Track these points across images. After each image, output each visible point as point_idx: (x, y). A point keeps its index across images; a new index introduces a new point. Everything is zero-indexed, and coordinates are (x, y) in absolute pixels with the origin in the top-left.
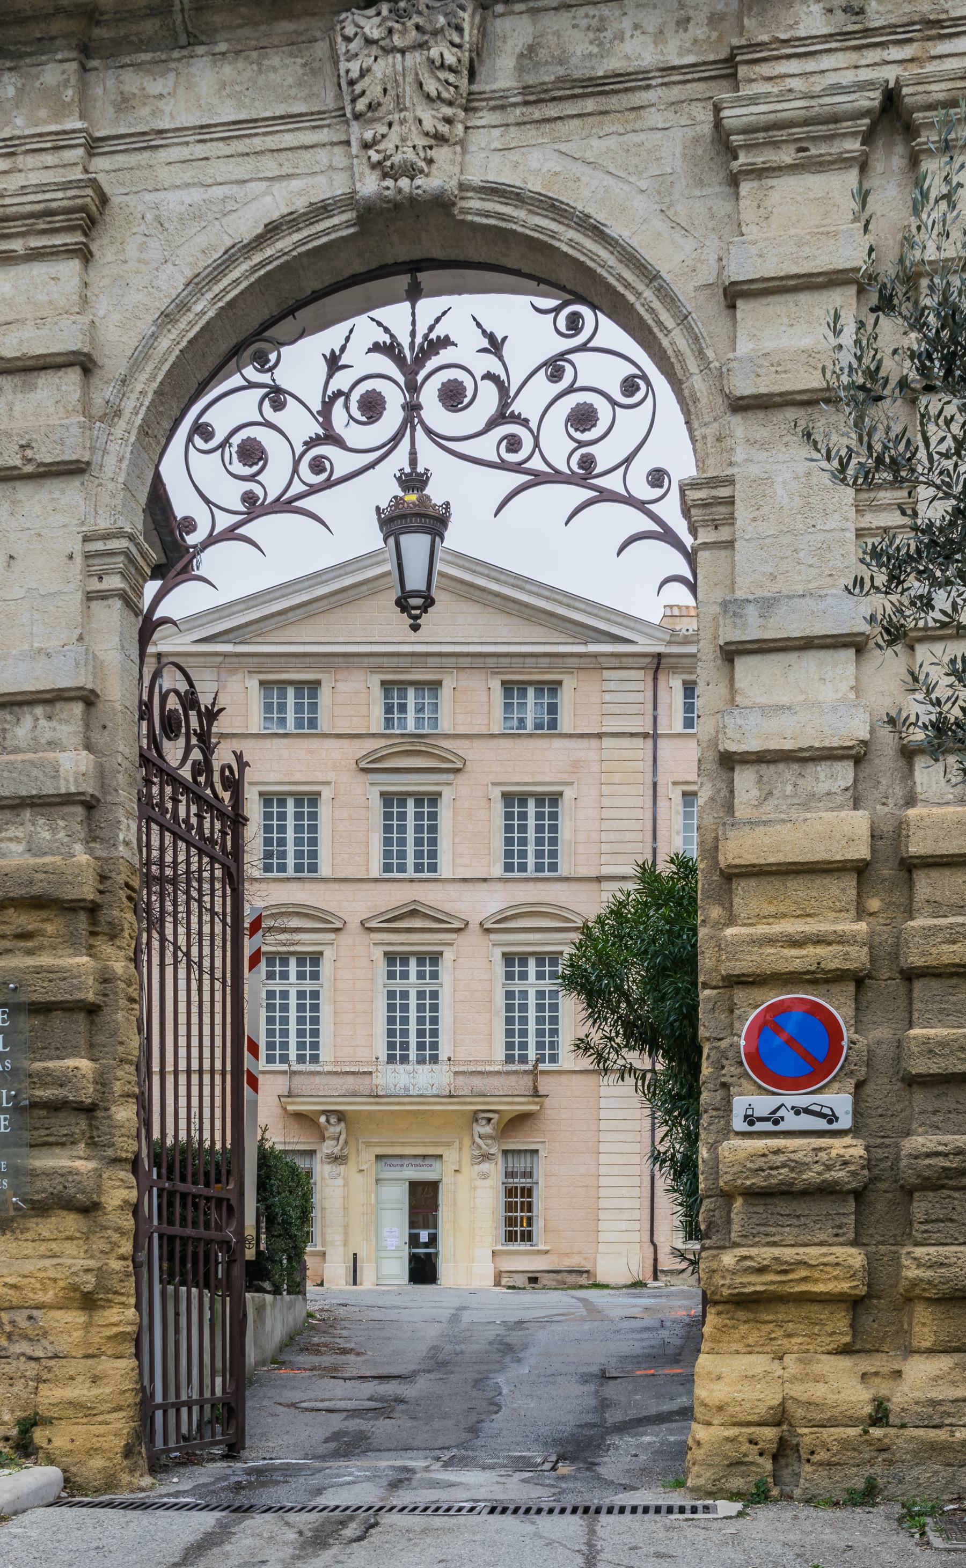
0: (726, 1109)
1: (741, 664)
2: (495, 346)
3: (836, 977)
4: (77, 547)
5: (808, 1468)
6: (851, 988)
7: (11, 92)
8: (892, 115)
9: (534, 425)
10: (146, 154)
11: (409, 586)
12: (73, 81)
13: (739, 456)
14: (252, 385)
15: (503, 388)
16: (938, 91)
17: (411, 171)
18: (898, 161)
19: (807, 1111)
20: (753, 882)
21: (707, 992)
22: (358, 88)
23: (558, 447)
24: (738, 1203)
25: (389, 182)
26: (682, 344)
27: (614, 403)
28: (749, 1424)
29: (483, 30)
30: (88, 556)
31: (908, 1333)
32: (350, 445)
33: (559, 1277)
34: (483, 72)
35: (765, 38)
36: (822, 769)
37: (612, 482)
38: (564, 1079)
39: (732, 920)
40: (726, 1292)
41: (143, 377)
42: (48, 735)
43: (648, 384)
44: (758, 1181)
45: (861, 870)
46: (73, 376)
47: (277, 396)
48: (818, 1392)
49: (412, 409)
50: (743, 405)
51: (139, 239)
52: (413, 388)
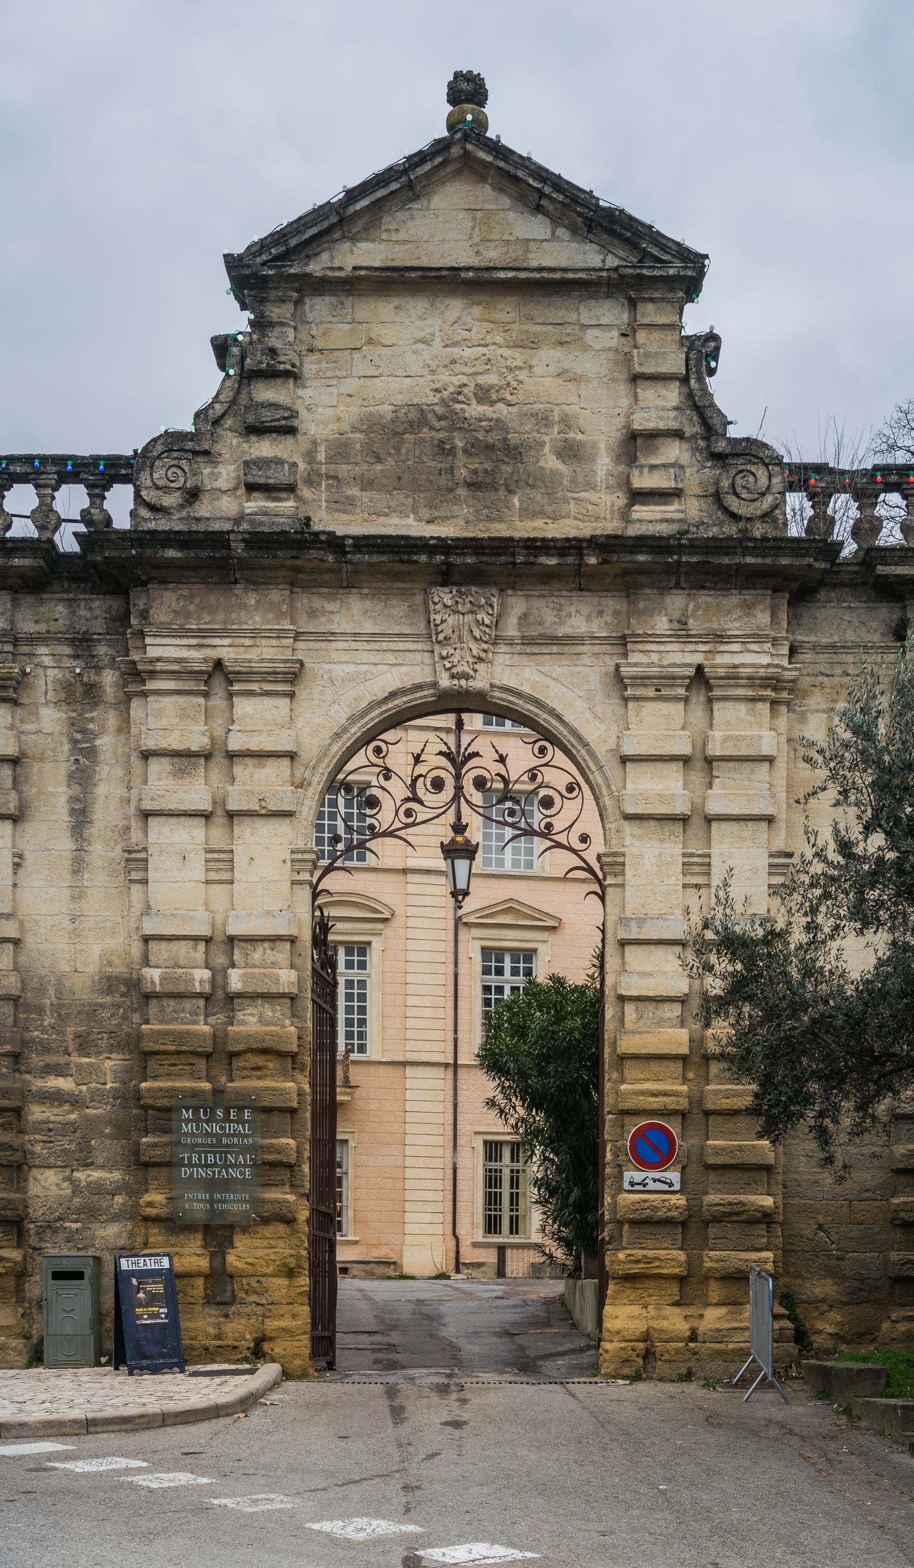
0: (620, 1177)
1: (628, 950)
2: (502, 759)
3: (674, 1113)
4: (288, 857)
5: (660, 1363)
6: (680, 1118)
7: (253, 602)
8: (700, 678)
10: (325, 643)
11: (458, 887)
12: (287, 601)
13: (628, 842)
16: (721, 672)
17: (467, 677)
18: (702, 699)
19: (659, 1180)
20: (633, 1062)
21: (610, 1116)
22: (440, 629)
24: (626, 1227)
25: (456, 682)
26: (600, 779)
27: (562, 796)
28: (631, 1341)
29: (502, 605)
30: (293, 861)
31: (706, 1295)
33: (368, 1268)
34: (501, 625)
35: (640, 632)
36: (667, 1006)
38: (372, 1069)
39: (623, 1081)
40: (620, 1273)
41: (323, 765)
42: (272, 959)
43: (580, 788)
44: (635, 1216)
45: (684, 1058)
46: (286, 762)
48: (664, 1324)
49: (459, 789)
50: (628, 817)
51: (321, 688)
52: (458, 777)
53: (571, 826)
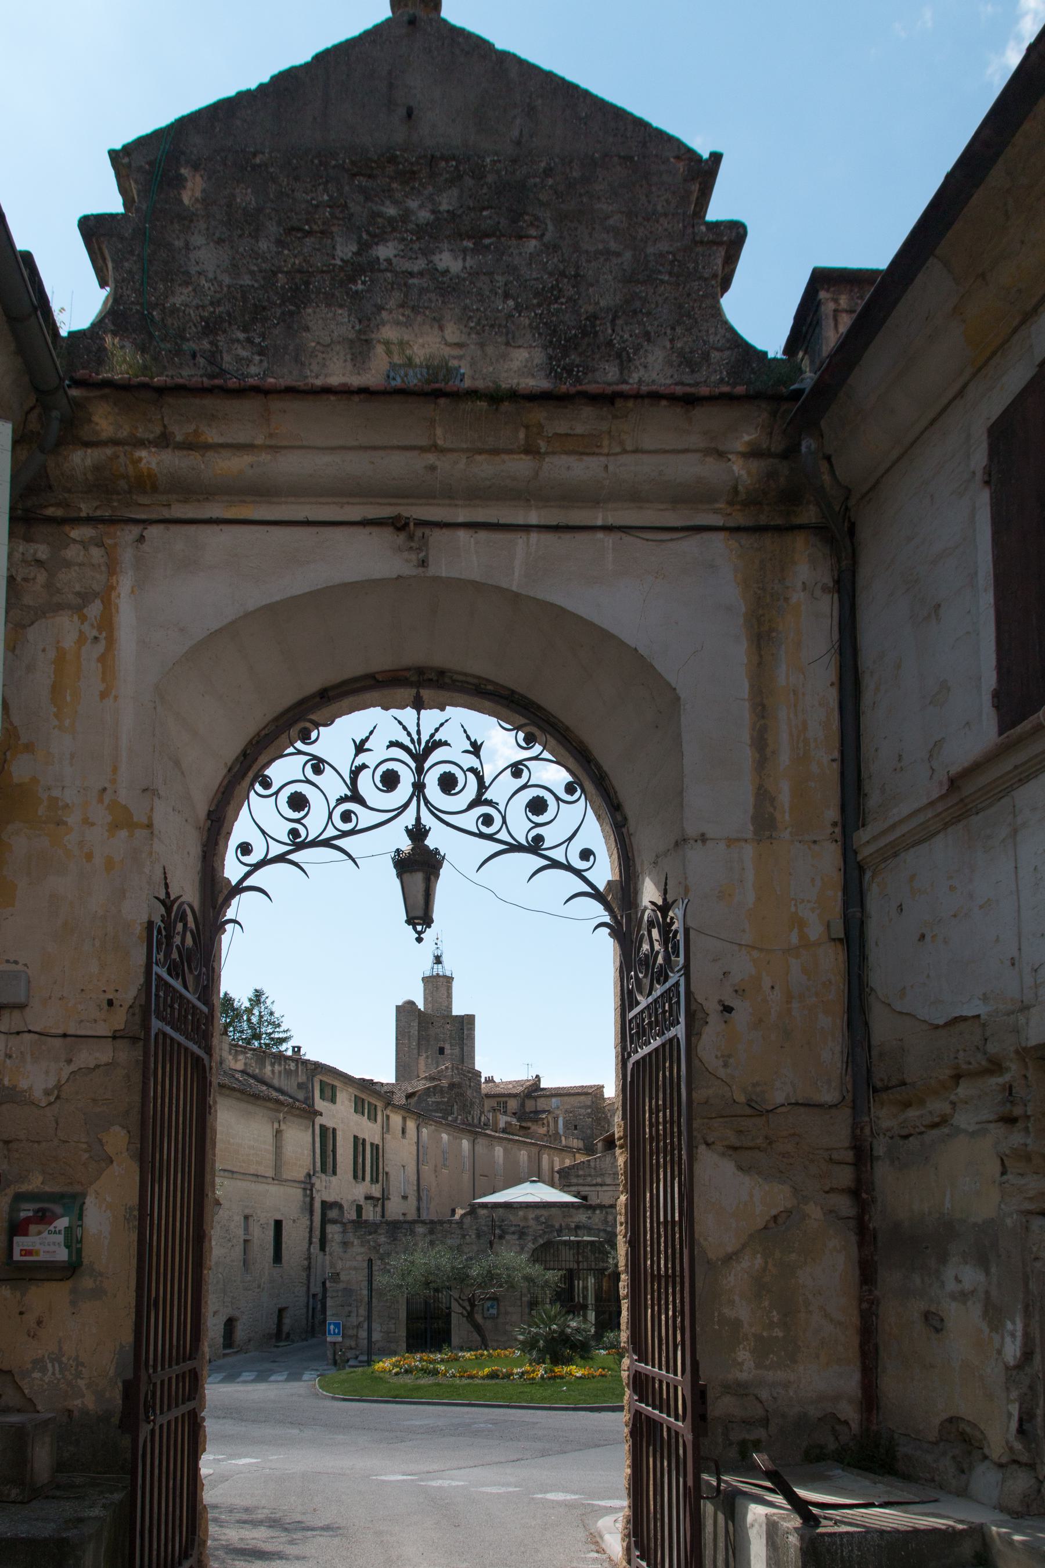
2: (476, 749)
9: (502, 808)
14: (300, 752)
15: (480, 779)
23: (520, 827)
27: (558, 799)
32: (369, 803)
37: (558, 855)
47: (318, 765)
49: (419, 787)
52: (420, 771)
53: (570, 839)
